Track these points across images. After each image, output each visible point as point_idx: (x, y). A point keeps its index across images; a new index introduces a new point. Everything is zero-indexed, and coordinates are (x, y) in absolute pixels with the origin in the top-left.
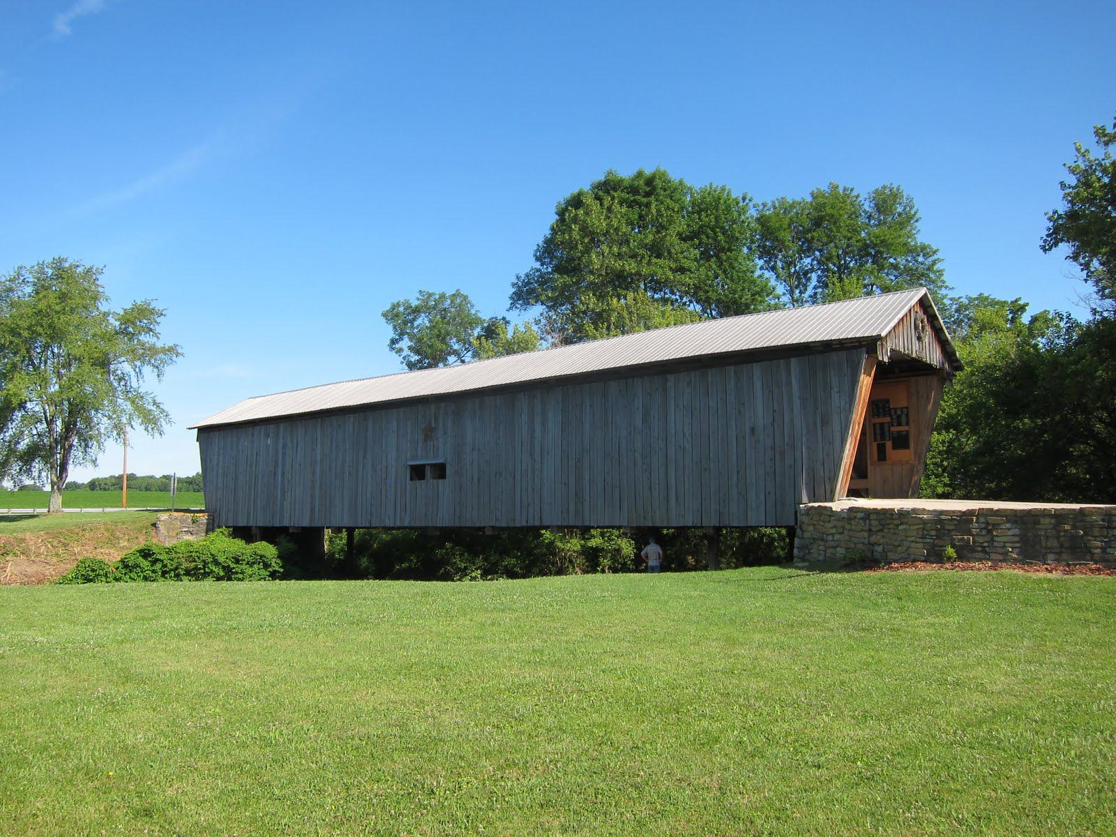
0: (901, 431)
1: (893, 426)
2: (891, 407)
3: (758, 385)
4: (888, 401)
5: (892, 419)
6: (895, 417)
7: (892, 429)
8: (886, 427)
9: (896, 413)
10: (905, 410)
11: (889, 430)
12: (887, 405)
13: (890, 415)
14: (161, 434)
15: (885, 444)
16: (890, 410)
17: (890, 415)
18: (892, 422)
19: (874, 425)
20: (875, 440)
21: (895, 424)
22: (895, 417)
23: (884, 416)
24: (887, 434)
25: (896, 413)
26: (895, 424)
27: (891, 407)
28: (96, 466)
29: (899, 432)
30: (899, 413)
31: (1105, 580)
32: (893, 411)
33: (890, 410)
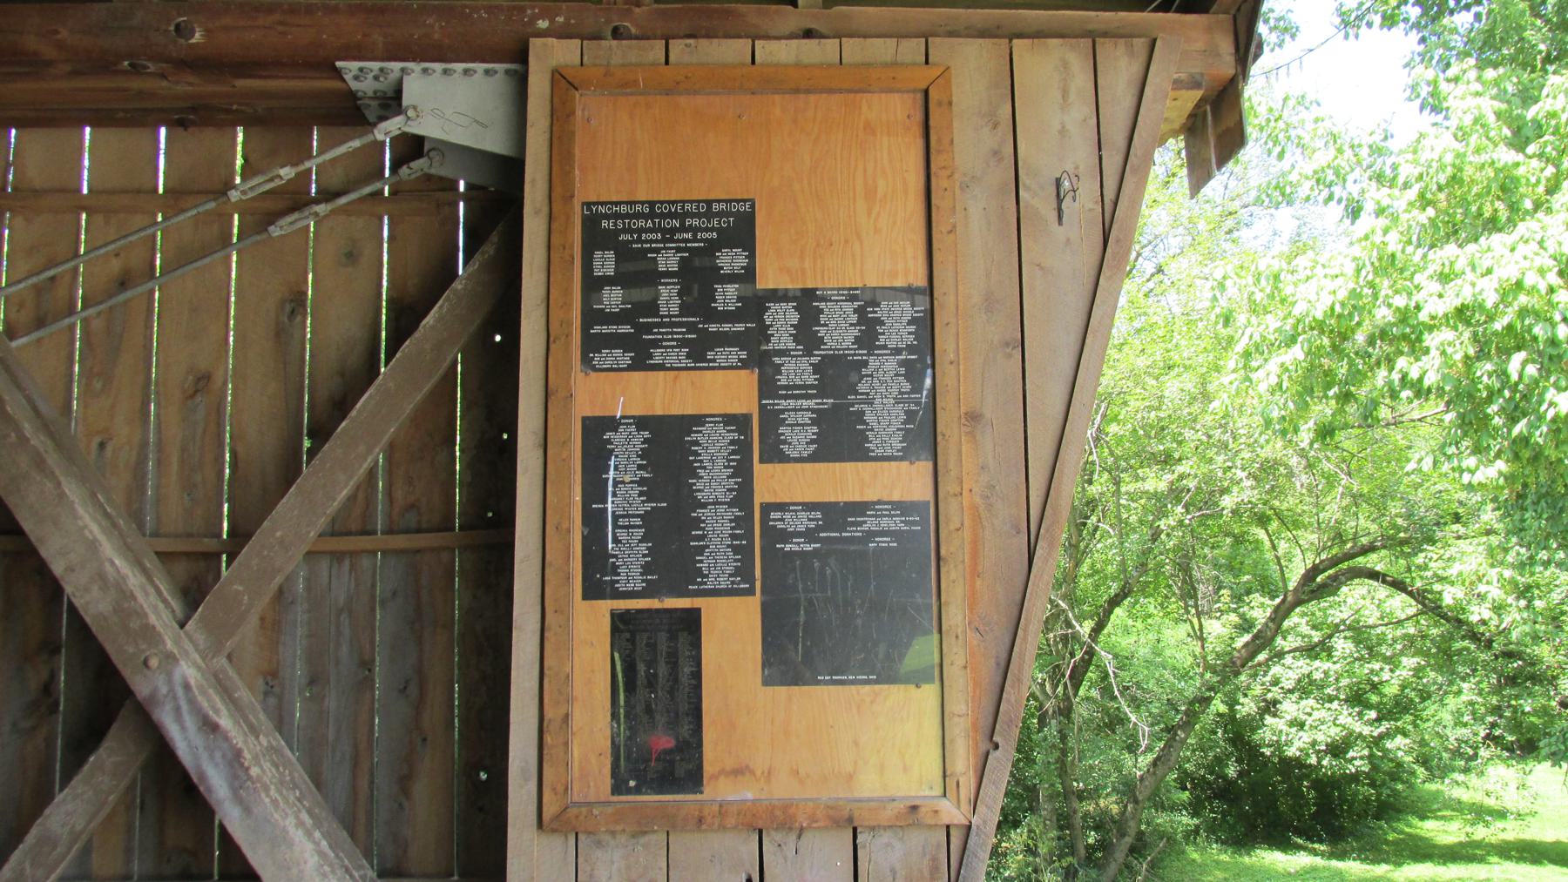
0: (860, 508)
1: (774, 453)
2: (768, 279)
3: (119, 759)
4: (741, 232)
5: (768, 387)
6: (797, 370)
7: (771, 483)
8: (713, 445)
9: (807, 336)
10: (898, 323)
11: (743, 496)
12: (732, 260)
13: (761, 360)
14: (1303, 97)
15: (690, 622)
16: (756, 305)
17: (761, 360)
18: (771, 420)
19: (597, 430)
20: (593, 591)
21: (799, 438)
22: (797, 370)
23: (699, 351)
24: (718, 524)
25: (807, 336)
26: (799, 438)
27: (768, 279)
28: (1294, 40)
29: (836, 514)
30: (838, 331)
31: (1565, 870)
32: (783, 319)
33: (756, 305)
